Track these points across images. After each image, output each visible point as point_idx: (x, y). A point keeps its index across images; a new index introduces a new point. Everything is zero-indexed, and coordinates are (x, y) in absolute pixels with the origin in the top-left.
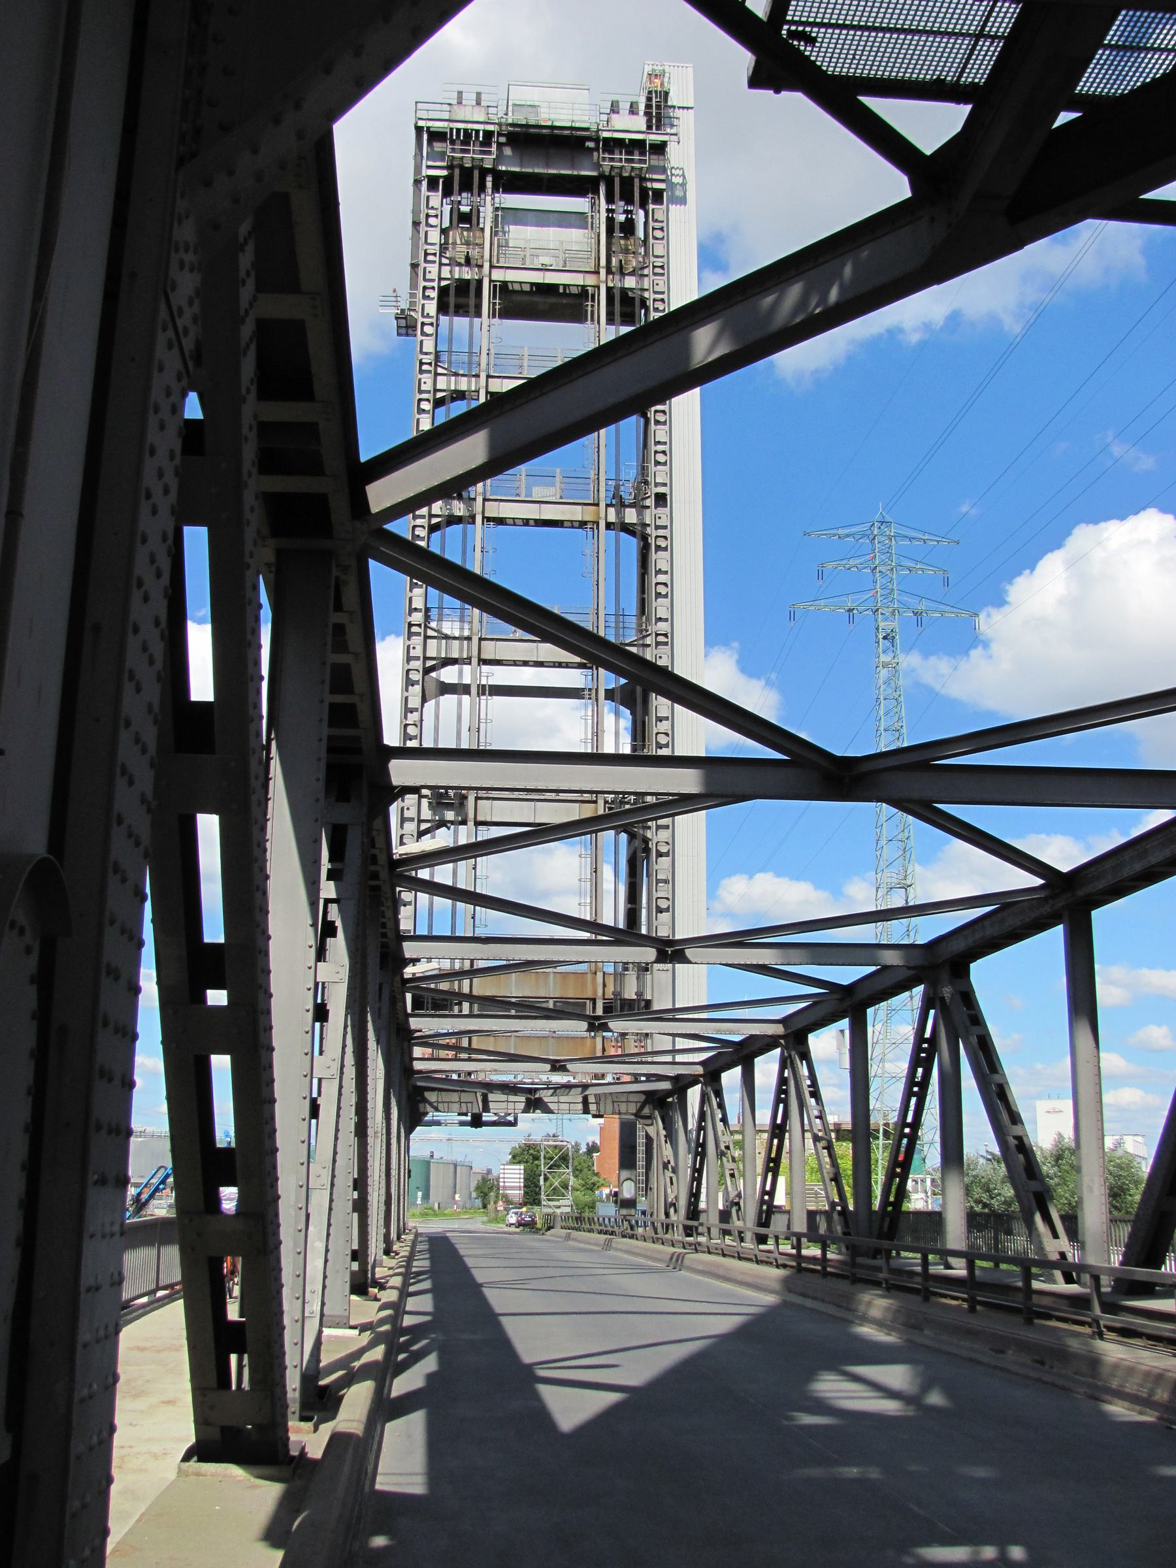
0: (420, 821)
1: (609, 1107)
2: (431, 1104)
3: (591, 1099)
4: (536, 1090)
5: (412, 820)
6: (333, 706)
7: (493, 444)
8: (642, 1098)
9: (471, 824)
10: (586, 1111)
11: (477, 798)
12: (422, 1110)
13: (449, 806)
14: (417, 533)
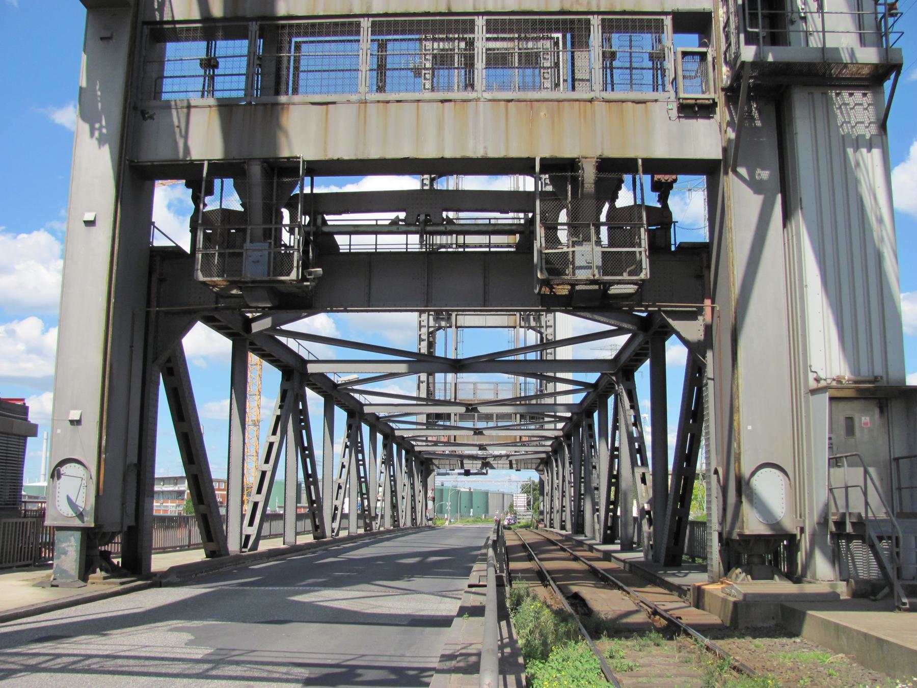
0: (429, 327)
1: (523, 466)
2: (436, 465)
3: (514, 462)
4: (486, 458)
5: (425, 326)
6: (534, 159)
7: (273, 321)
8: (539, 461)
9: (454, 328)
10: (511, 467)
11: (456, 315)
12: (431, 468)
13: (443, 319)
14: (424, 182)
